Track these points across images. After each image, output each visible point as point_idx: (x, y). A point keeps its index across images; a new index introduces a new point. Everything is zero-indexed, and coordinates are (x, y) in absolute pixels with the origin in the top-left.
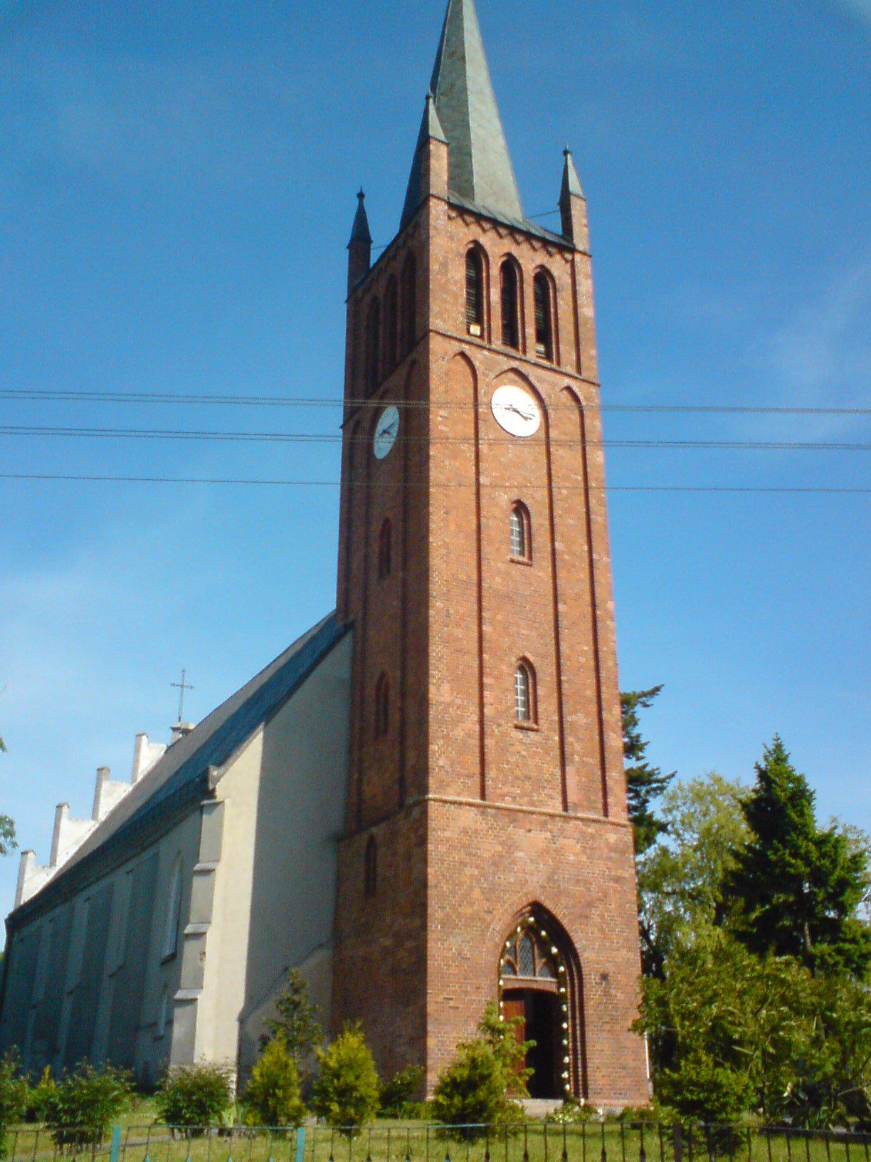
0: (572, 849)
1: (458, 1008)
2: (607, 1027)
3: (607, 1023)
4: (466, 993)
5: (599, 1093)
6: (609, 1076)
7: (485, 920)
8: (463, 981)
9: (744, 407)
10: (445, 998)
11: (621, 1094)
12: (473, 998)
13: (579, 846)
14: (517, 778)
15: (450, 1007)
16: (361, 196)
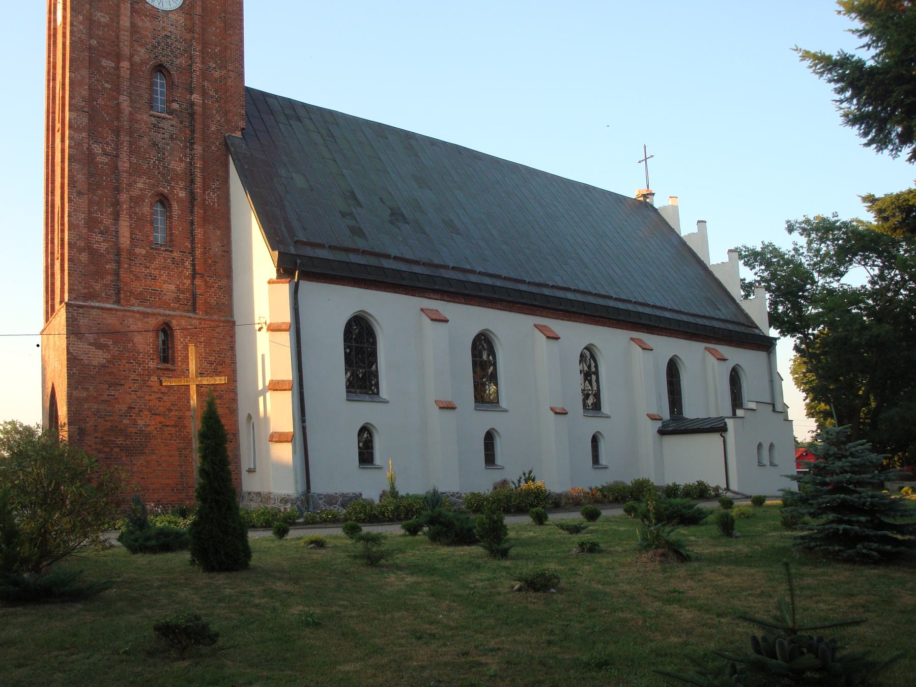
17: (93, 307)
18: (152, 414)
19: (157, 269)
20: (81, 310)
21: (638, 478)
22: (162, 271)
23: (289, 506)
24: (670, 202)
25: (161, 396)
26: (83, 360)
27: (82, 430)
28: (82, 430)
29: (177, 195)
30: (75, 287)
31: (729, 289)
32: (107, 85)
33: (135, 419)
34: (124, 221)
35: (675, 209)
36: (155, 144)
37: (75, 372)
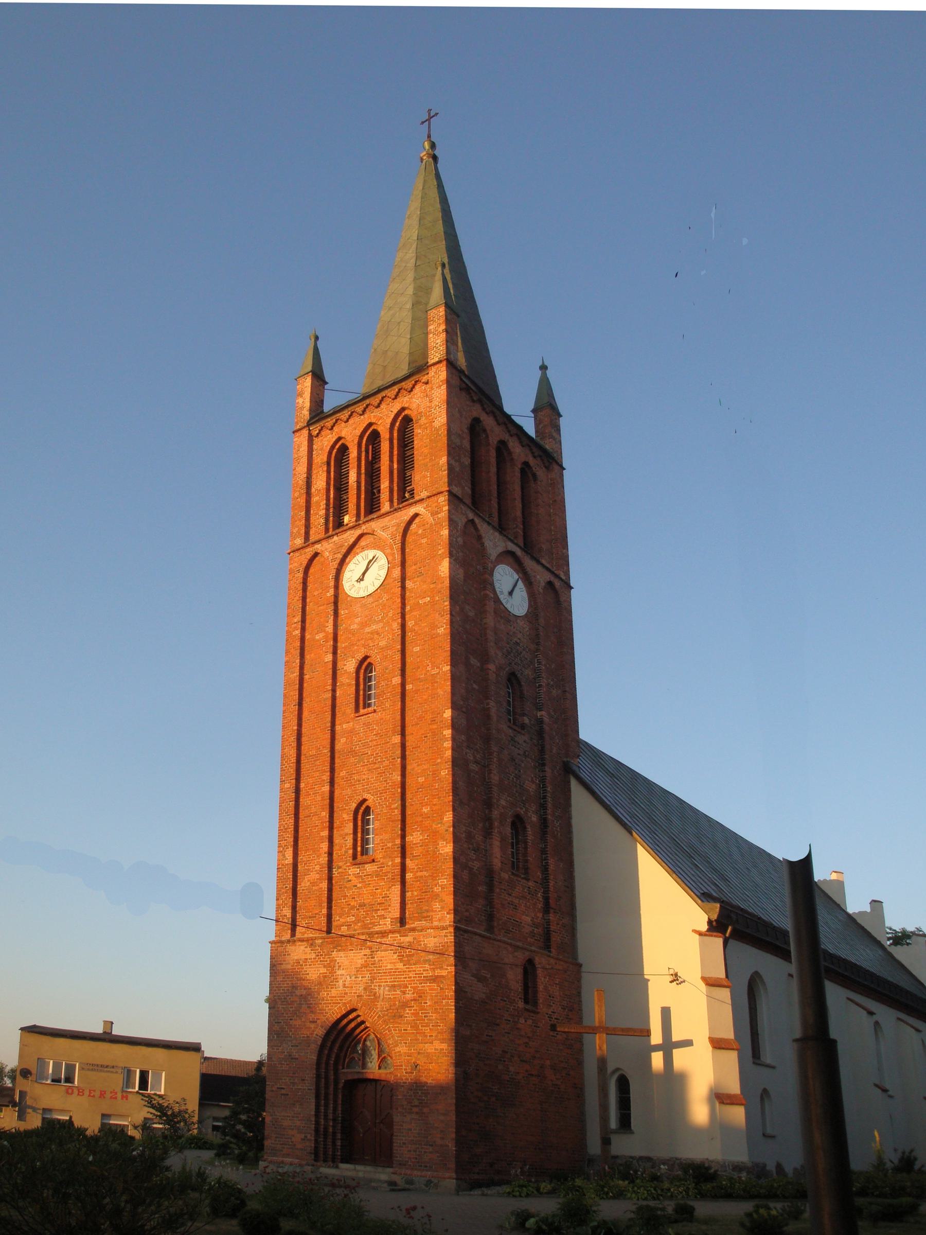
0: (388, 959)
1: (288, 1095)
2: (415, 1110)
3: (416, 1106)
4: (294, 1084)
5: (405, 1165)
6: (415, 1151)
7: (310, 1028)
8: (292, 1075)
9: (305, 476)
10: (278, 1088)
11: (426, 1166)
12: (300, 1087)
13: (395, 956)
14: (353, 908)
15: (282, 1094)
16: (544, 368)
17: (476, 934)
18: (521, 1061)
19: (518, 898)
20: (466, 936)
21: (85, 1125)
22: (521, 901)
23: (744, 1176)
24: (834, 876)
25: (527, 1040)
26: (467, 992)
27: (466, 1074)
28: (466, 1074)
29: (531, 818)
30: (459, 908)
31: (914, 973)
32: (475, 686)
33: (507, 1065)
34: (496, 840)
35: (840, 884)
36: (513, 760)
37: (461, 1005)
